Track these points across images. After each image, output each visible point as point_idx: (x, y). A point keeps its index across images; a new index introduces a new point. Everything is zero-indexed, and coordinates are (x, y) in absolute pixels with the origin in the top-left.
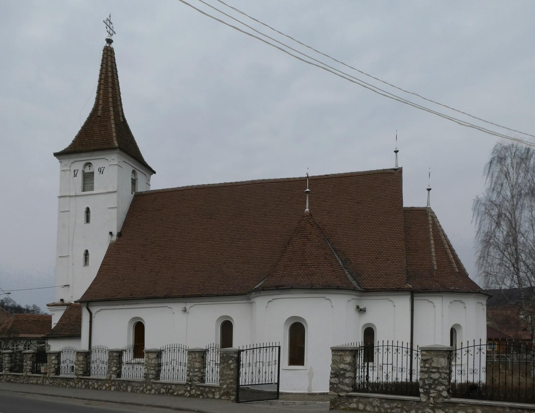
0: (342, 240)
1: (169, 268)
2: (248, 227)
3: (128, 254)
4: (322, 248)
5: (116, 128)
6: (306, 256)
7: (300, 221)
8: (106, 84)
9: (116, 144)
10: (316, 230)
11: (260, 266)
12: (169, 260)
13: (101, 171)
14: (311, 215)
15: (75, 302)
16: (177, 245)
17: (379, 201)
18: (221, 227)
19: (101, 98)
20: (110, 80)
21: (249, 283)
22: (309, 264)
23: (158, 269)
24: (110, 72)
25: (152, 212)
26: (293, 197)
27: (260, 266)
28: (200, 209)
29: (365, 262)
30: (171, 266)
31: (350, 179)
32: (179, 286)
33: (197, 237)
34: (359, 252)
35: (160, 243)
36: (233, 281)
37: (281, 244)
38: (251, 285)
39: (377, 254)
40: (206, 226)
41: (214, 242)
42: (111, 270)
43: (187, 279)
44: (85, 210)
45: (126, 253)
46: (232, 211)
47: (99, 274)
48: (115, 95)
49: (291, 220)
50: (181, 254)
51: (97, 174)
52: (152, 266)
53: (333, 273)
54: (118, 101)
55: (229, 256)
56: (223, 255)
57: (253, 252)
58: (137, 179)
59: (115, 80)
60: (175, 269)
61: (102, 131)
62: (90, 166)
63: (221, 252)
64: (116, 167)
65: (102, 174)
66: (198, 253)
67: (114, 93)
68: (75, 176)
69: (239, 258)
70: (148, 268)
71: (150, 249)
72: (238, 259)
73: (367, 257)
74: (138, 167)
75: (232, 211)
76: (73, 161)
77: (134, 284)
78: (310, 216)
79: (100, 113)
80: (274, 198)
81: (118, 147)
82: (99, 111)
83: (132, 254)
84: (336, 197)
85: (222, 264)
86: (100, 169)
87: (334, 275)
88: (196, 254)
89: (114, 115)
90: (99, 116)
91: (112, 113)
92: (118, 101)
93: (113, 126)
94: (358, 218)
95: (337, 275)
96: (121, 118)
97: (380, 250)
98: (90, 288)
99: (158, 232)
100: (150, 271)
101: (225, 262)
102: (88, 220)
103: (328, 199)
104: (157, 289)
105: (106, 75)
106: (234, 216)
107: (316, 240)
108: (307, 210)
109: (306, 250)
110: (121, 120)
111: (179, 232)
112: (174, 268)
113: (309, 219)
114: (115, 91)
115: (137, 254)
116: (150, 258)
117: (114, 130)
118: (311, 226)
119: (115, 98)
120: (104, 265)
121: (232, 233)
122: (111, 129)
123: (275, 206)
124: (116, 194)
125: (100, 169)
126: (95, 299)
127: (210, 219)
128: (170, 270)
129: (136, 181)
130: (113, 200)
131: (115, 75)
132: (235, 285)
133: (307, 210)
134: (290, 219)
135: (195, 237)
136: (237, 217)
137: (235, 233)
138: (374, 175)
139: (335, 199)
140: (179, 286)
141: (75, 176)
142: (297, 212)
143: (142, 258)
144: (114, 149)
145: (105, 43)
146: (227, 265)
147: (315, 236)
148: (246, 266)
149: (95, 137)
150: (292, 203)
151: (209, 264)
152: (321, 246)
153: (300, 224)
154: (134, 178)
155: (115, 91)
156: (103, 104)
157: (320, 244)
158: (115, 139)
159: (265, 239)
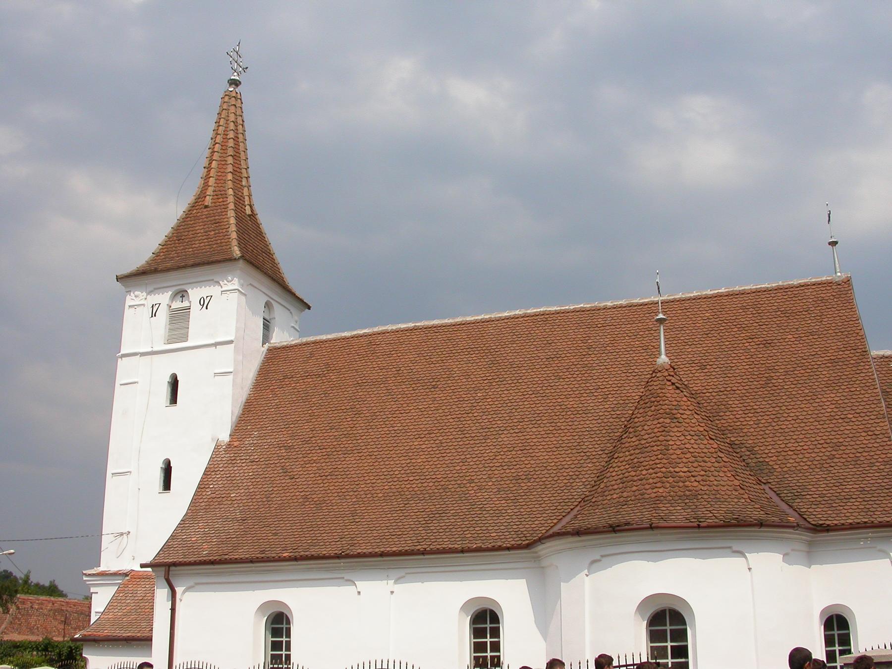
0: (744, 423)
1: (345, 494)
2: (520, 404)
3: (254, 467)
4: (707, 437)
5: (237, 225)
6: (673, 457)
7: (648, 382)
8: (222, 151)
9: (237, 252)
10: (690, 399)
11: (556, 486)
12: (345, 476)
13: (204, 303)
14: (674, 369)
15: (142, 566)
16: (362, 444)
17: (813, 340)
18: (460, 406)
19: (211, 175)
20: (231, 143)
21: (536, 523)
22: (681, 474)
23: (320, 495)
24: (232, 131)
25: (305, 381)
26: (616, 339)
27: (556, 486)
28: (410, 371)
29: (806, 467)
30: (349, 490)
31: (739, 299)
32: (369, 532)
33: (406, 428)
34: (787, 446)
35: (324, 441)
36: (495, 518)
37: (601, 435)
38: (540, 525)
39: (829, 449)
40: (424, 403)
41: (445, 437)
42: (219, 500)
43: (388, 516)
44: (168, 379)
45: (250, 464)
46: (481, 372)
47: (192, 509)
48: (238, 170)
49: (619, 385)
50: (371, 464)
51: (195, 307)
52: (306, 490)
53: (742, 491)
54: (244, 178)
55: (481, 466)
56: (466, 464)
57: (537, 455)
58: (275, 318)
59: (241, 144)
60: (359, 496)
61: (210, 231)
62: (183, 296)
63: (463, 457)
64: (236, 294)
65: (207, 308)
66: (409, 461)
67: (236, 165)
68: (154, 315)
69: (505, 468)
70: (297, 494)
71: (301, 456)
72: (503, 471)
73: (807, 455)
74: (276, 296)
75: (481, 372)
76: (152, 289)
77: (268, 528)
78: (672, 370)
79: (208, 201)
80: (575, 342)
81: (241, 257)
82: (208, 197)
83: (263, 467)
84: (716, 335)
85: (465, 482)
86: (202, 300)
87: (744, 496)
88: (404, 462)
89: (235, 204)
90: (206, 207)
91: (231, 199)
92: (244, 178)
93: (233, 221)
94: (773, 375)
95: (751, 496)
96: (248, 208)
97: (835, 441)
98: (173, 537)
99: (319, 420)
100: (301, 500)
101: (473, 478)
102: (174, 399)
103: (696, 340)
104: (320, 538)
105: (225, 137)
106: (485, 382)
107: (692, 421)
108: (663, 359)
109: (671, 443)
110: (247, 212)
111: (365, 418)
112: (356, 494)
113: (669, 375)
114: (238, 162)
115: (272, 466)
116: (301, 473)
117: (233, 228)
118: (677, 391)
119: (238, 174)
120: (203, 490)
121: (484, 417)
122: (227, 226)
123: (577, 357)
124: (233, 345)
125: (202, 300)
126: (185, 560)
127: (433, 390)
128: (348, 497)
129: (272, 321)
130: (225, 358)
131: (241, 135)
132: (501, 528)
133: (663, 359)
134: (616, 382)
135: (400, 428)
136: (494, 384)
137: (490, 417)
138: (791, 290)
139: (714, 338)
140: (369, 532)
141: (154, 315)
142: (629, 368)
143: (285, 474)
144: (231, 260)
145: (225, 86)
146: (479, 484)
147: (688, 412)
148: (522, 485)
149: (197, 242)
150: (617, 351)
151: (436, 484)
152: (706, 433)
153: (650, 388)
154: (267, 318)
155: (238, 162)
156: (216, 185)
157: (702, 429)
158: (235, 243)
159: (562, 427)
